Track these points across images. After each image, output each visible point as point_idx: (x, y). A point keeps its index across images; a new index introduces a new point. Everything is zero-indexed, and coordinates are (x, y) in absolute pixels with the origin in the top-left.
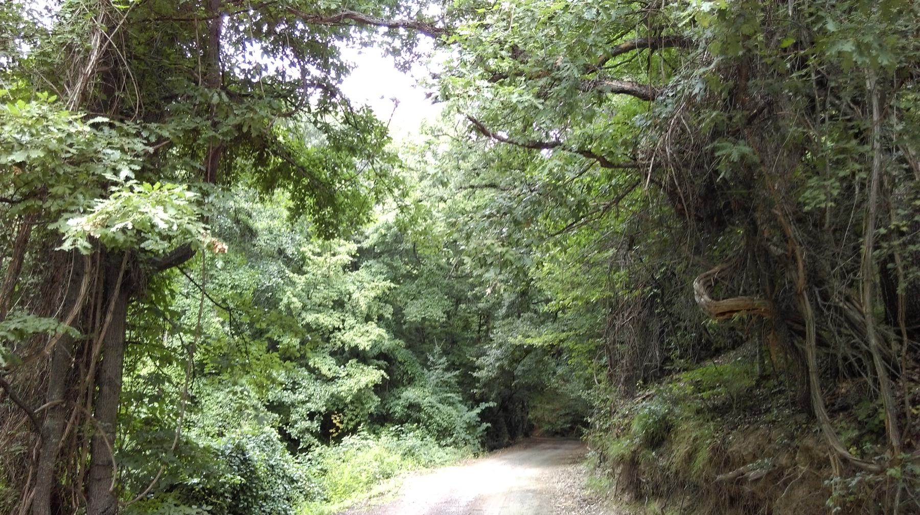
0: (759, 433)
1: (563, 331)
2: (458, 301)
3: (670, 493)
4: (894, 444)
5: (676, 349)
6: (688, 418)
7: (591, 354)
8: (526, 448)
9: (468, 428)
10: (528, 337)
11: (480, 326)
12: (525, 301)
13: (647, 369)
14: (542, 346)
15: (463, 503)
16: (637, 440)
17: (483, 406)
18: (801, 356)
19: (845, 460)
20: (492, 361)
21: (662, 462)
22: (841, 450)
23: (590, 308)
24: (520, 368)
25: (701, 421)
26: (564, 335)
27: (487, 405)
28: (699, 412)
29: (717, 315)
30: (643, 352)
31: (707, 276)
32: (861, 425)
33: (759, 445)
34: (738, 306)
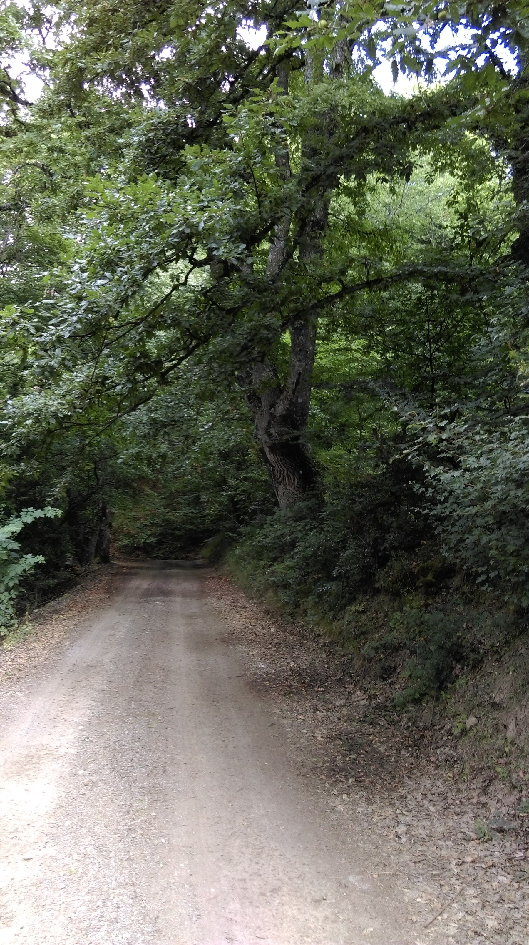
17: (30, 515)
27: (39, 513)
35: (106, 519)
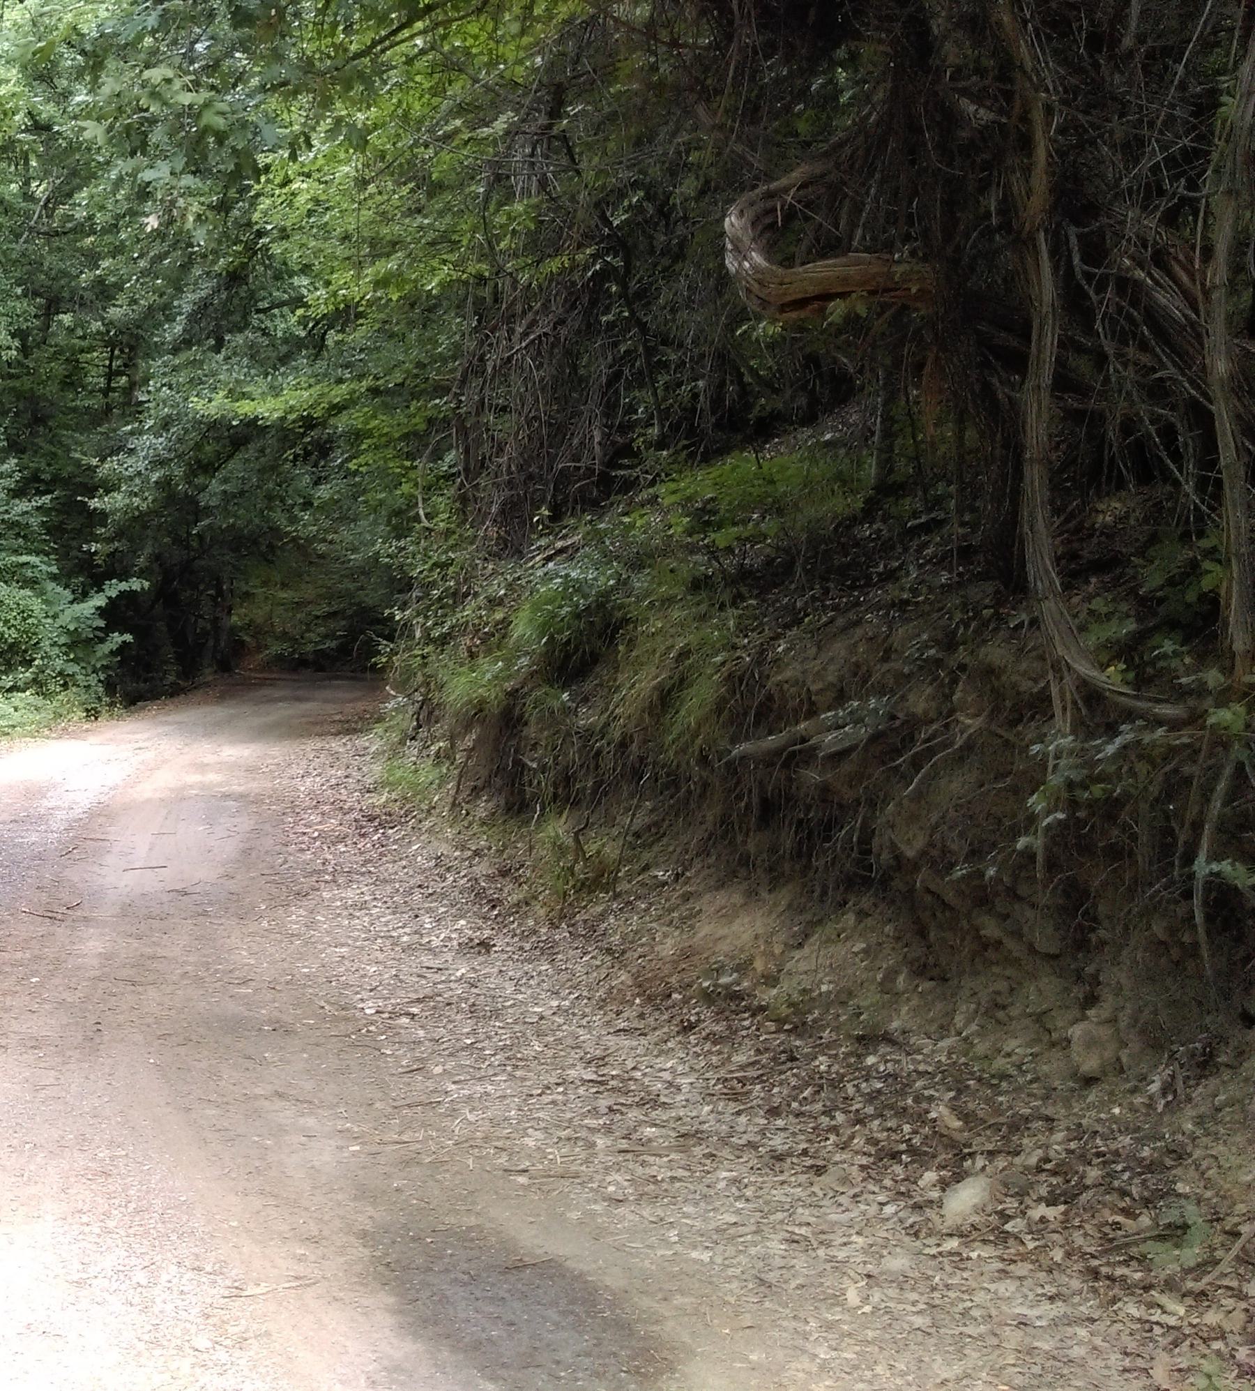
0: (859, 632)
1: (340, 381)
2: (53, 306)
3: (600, 792)
4: (1238, 646)
5: (649, 425)
6: (668, 601)
7: (415, 443)
8: (222, 698)
9: (71, 646)
10: (244, 396)
11: (111, 375)
12: (239, 297)
13: (564, 478)
14: (283, 419)
15: (58, 821)
16: (524, 661)
17: (114, 588)
18: (1004, 423)
19: (1092, 696)
20: (141, 466)
21: (587, 718)
22: (1085, 669)
23: (423, 310)
24: (215, 486)
25: (703, 608)
26: (339, 393)
27: (124, 586)
28: (698, 584)
29: (783, 308)
30: (559, 431)
31: (770, 195)
32: (1146, 605)
33: (857, 665)
34: (845, 280)
35: (223, 600)
